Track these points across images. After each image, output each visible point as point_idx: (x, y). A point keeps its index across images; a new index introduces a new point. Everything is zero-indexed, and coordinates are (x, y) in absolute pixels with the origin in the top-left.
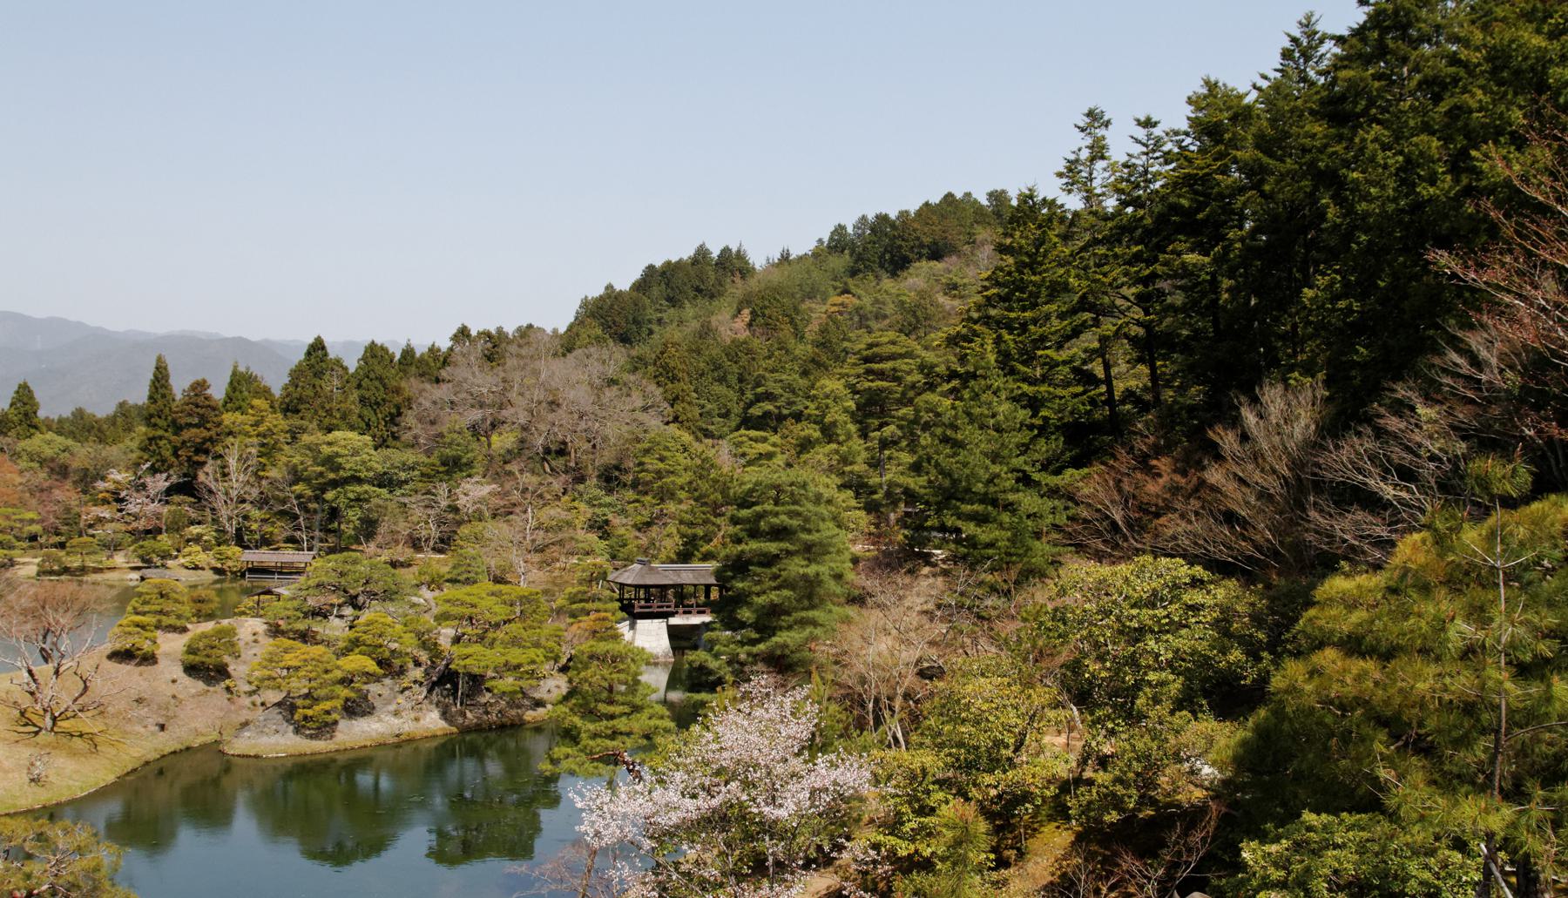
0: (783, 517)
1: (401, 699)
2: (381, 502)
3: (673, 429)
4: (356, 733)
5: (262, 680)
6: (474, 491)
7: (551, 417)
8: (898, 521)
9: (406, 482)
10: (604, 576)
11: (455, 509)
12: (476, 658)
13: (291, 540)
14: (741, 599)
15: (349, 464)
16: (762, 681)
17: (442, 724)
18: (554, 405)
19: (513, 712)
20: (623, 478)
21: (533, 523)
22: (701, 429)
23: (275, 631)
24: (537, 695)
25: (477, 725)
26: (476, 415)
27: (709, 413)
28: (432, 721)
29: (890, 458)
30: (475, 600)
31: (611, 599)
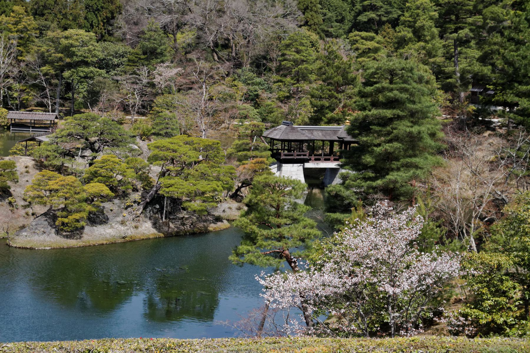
0: (396, 92)
1: (125, 213)
2: (101, 79)
3: (304, 30)
4: (96, 235)
5: (34, 198)
6: (166, 73)
7: (219, 21)
8: (467, 98)
9: (118, 65)
10: (260, 134)
11: (152, 85)
12: (178, 187)
13: (41, 105)
14: (364, 149)
15: (80, 52)
16: (384, 205)
17: (154, 231)
18: (221, 12)
19: (201, 225)
20: (270, 65)
21: (206, 96)
22: (323, 31)
23: (40, 166)
24: (216, 214)
25: (177, 232)
26: (166, 19)
27: (329, 19)
28: (147, 229)
29: (460, 53)
30: (176, 147)
31: (265, 149)
